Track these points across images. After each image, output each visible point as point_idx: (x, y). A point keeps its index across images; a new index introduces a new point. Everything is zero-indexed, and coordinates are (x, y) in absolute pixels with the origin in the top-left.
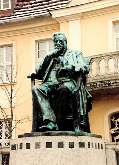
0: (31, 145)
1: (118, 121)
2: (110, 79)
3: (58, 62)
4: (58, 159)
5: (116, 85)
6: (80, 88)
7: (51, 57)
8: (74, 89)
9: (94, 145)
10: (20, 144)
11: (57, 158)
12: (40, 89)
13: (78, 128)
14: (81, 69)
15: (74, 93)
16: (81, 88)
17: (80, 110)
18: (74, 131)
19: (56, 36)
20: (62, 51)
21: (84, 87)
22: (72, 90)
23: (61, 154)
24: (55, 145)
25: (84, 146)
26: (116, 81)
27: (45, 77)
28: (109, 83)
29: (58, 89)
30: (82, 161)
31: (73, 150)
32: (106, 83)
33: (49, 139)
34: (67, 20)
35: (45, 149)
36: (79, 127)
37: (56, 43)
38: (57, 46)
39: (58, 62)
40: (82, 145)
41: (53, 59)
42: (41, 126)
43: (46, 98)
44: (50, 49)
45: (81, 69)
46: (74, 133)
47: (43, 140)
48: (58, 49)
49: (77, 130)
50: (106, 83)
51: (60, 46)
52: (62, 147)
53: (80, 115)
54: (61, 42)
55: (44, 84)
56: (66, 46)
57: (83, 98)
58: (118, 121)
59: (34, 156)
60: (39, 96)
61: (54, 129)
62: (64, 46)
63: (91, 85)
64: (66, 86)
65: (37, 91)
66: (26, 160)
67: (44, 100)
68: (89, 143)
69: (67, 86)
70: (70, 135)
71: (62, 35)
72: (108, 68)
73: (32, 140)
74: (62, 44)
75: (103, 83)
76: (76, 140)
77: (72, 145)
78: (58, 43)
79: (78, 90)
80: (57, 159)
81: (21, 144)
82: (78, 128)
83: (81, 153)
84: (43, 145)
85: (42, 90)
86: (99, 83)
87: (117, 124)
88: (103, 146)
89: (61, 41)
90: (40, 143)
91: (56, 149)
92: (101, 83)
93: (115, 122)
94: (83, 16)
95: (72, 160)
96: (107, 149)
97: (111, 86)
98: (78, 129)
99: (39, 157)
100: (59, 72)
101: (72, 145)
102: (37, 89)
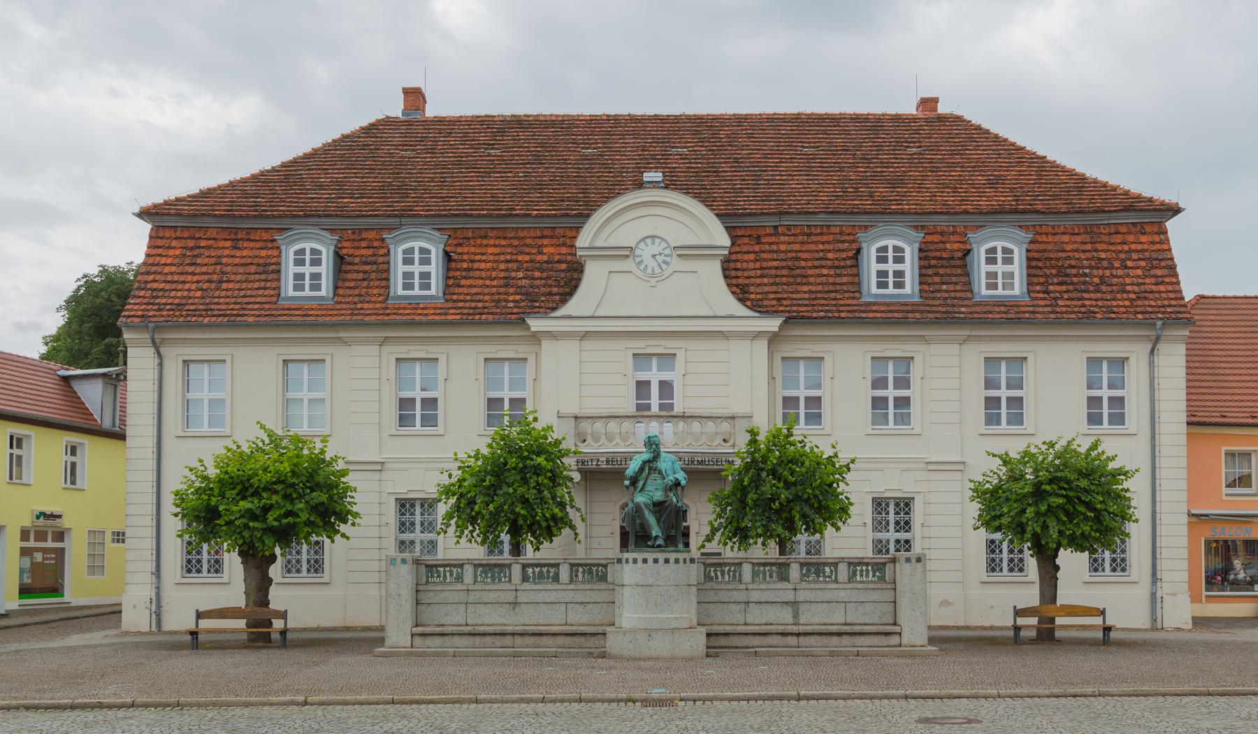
24: (672, 561)
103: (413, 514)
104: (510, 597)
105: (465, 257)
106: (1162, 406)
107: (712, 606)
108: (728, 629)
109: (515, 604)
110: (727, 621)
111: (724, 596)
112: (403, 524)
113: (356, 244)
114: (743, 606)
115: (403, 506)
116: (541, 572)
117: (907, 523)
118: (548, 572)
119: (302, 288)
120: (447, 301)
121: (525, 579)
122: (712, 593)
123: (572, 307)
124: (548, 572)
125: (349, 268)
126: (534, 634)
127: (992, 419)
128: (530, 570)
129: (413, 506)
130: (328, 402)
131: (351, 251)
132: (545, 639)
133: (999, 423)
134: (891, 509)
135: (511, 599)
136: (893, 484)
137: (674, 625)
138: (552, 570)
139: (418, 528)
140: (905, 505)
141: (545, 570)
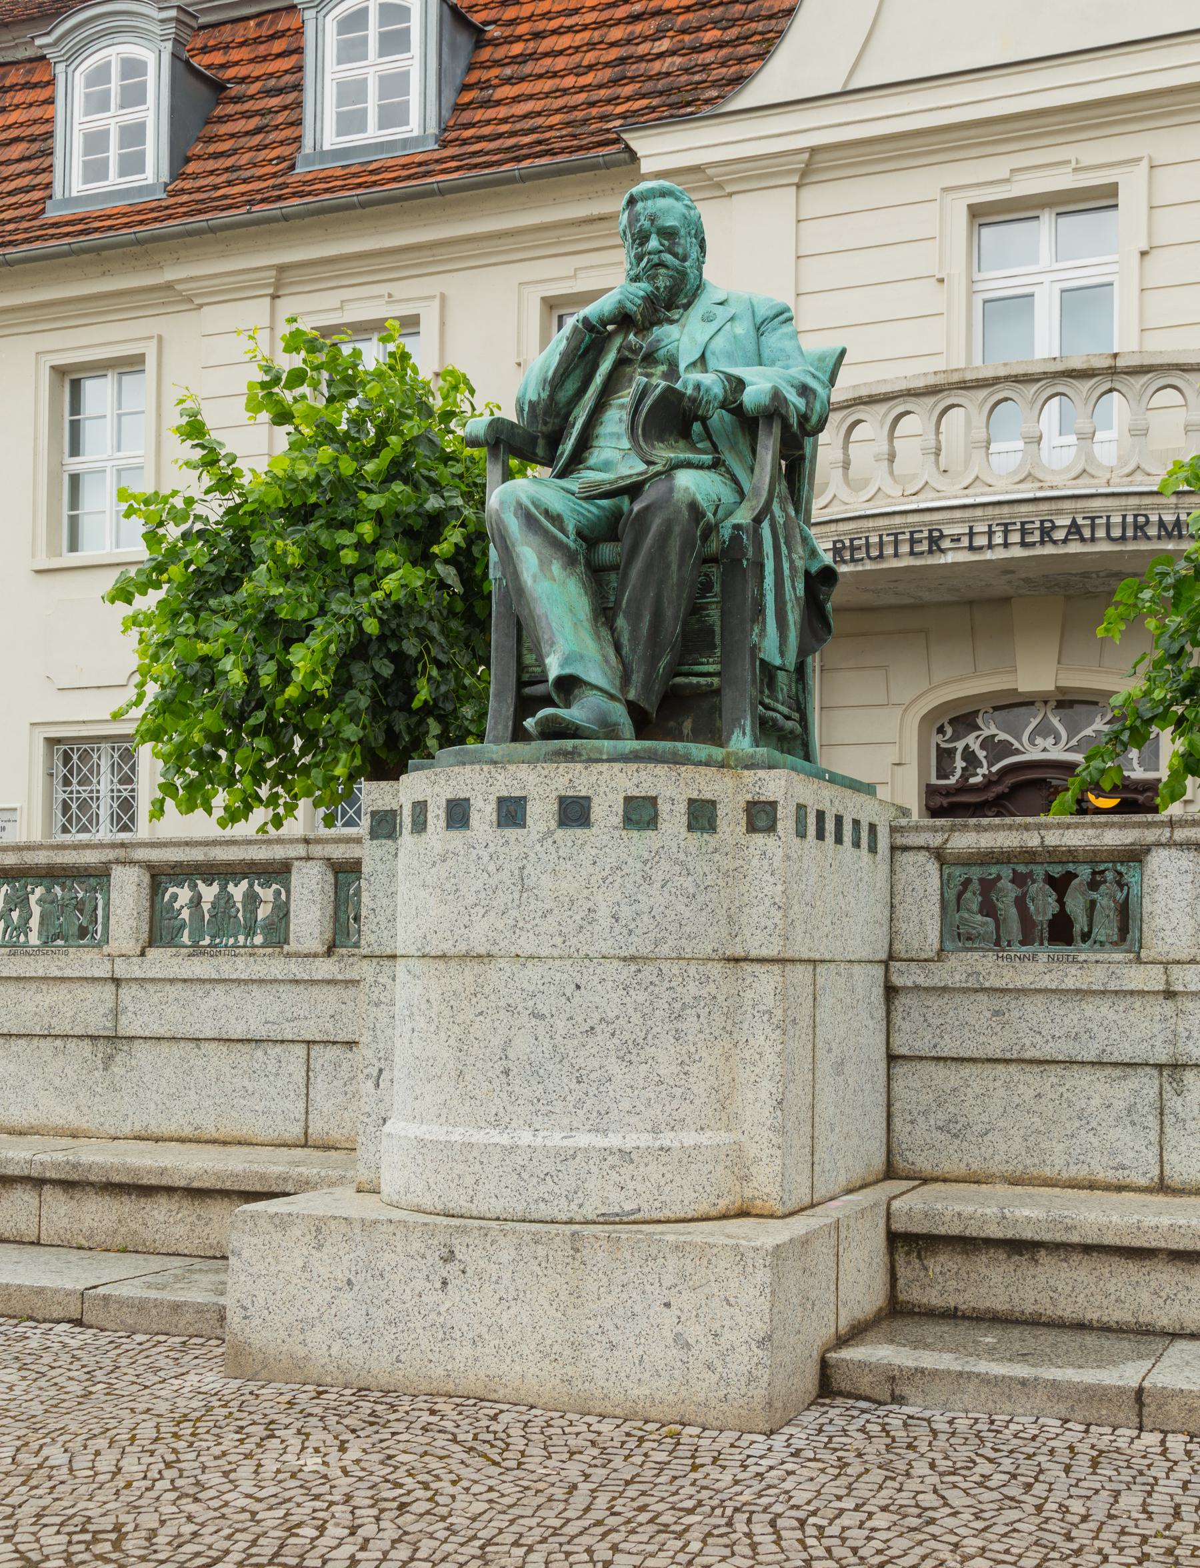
1: (967, 746)
3: (650, 359)
4: (622, 886)
5: (971, 548)
6: (767, 509)
7: (610, 328)
8: (730, 514)
9: (830, 826)
10: (416, 804)
11: (619, 880)
12: (537, 507)
13: (748, 729)
14: (777, 395)
15: (732, 538)
16: (776, 507)
18: (720, 742)
19: (639, 206)
20: (671, 288)
21: (793, 513)
22: (720, 513)
23: (639, 865)
24: (607, 810)
25: (771, 828)
26: (971, 528)
27: (568, 446)
29: (637, 507)
30: (755, 902)
31: (707, 843)
32: (916, 536)
34: (719, 186)
36: (753, 730)
37: (641, 244)
38: (643, 264)
39: (650, 359)
40: (761, 816)
41: (617, 342)
42: (533, 715)
43: (570, 559)
44: (608, 279)
45: (777, 395)
46: (718, 753)
48: (652, 279)
49: (742, 742)
50: (916, 536)
51: (661, 264)
53: (762, 661)
55: (564, 483)
56: (700, 269)
57: (787, 572)
58: (967, 746)
59: (492, 868)
60: (528, 545)
61: (610, 731)
62: (687, 264)
64: (687, 489)
66: (448, 886)
67: (556, 568)
68: (801, 807)
69: (693, 488)
70: (699, 763)
72: (937, 462)
74: (675, 255)
75: (900, 537)
76: (729, 792)
78: (654, 243)
79: (757, 520)
80: (616, 884)
81: (420, 808)
83: (755, 862)
85: (546, 513)
86: (881, 536)
87: (964, 758)
88: (880, 835)
89: (668, 234)
91: (616, 834)
92: (892, 538)
93: (956, 749)
94: (812, 166)
95: (701, 899)
96: (901, 1001)
97: (942, 551)
99: (517, 872)
100: (649, 402)
101: (702, 815)
102: (520, 505)
104: (90, 1009)
105: (522, 29)
107: (975, 1079)
108: (1029, 1213)
109: (113, 1041)
110: (1057, 1163)
111: (1041, 1028)
113: (262, 50)
114: (1147, 1085)
116: (225, 899)
118: (252, 899)
120: (444, 144)
121: (160, 931)
122: (978, 1010)
123: (773, 80)
124: (252, 899)
125: (231, 109)
126: (112, 1188)
128: (184, 895)
131: (242, 71)
132: (160, 1211)
135: (98, 1023)
137: (602, 1195)
138: (267, 894)
141: (238, 891)
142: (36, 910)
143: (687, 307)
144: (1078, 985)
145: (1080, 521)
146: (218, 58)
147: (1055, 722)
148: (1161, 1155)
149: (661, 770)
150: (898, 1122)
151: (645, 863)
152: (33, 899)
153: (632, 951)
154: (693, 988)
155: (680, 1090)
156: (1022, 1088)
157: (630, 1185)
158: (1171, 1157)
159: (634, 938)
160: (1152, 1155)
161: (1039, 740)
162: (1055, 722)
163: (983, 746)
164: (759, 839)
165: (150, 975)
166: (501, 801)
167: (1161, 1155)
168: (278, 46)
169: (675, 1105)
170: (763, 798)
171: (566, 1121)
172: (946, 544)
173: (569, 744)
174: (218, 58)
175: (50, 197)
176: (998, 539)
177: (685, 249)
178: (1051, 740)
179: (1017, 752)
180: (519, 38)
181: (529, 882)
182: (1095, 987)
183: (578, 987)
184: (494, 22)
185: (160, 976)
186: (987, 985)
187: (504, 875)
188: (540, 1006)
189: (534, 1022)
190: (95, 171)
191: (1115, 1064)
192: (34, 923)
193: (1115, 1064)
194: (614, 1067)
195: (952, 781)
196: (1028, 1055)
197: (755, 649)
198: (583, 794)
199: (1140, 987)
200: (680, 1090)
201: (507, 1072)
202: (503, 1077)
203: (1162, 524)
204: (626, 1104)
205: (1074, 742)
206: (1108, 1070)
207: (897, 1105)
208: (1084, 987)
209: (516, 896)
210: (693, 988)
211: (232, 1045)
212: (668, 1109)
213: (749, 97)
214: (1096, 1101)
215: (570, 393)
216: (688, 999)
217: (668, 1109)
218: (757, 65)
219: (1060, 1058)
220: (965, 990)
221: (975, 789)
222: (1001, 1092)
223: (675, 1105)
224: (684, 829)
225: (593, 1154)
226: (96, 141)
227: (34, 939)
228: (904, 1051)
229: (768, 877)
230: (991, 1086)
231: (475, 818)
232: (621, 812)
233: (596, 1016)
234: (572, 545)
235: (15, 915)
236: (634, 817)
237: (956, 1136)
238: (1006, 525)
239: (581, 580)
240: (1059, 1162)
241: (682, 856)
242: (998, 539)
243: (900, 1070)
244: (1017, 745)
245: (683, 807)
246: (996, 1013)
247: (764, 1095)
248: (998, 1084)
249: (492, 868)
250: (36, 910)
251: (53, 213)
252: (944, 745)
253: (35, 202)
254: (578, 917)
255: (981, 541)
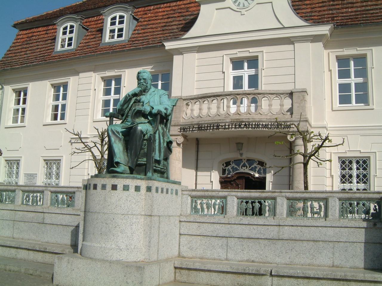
0: (97, 186)
2: (220, 121)
10: (168, 193)
12: (114, 130)
13: (151, 172)
17: (155, 154)
23: (125, 197)
24: (120, 187)
25: (150, 191)
26: (225, 124)
28: (259, 124)
33: (115, 181)
35: (110, 191)
47: (109, 181)
52: (128, 190)
53: (155, 159)
54: (144, 81)
59: (100, 197)
63: (199, 126)
65: (111, 131)
67: (117, 142)
71: (147, 73)
73: (100, 182)
76: (143, 184)
77: (137, 189)
78: (142, 81)
82: (151, 172)
84: (109, 187)
87: (236, 168)
90: (106, 185)
91: (122, 192)
93: (226, 169)
98: (151, 173)
101: (137, 189)
103: (351, 169)
106: (371, 89)
112: (343, 176)
113: (96, 22)
115: (343, 162)
117: (365, 176)
119: (113, 37)
121: (292, 211)
123: (193, 31)
127: (344, 99)
129: (351, 162)
130: (15, 125)
133: (350, 102)
134: (355, 166)
136: (356, 147)
139: (355, 180)
140: (364, 163)
142: (31, 198)
143: (147, 92)
144: (213, 222)
145: (247, 124)
146: (88, 24)
147: (246, 164)
148: (227, 254)
149: (130, 180)
150: (181, 247)
151: (126, 197)
152: (31, 196)
153: (123, 213)
154: (134, 220)
155: (131, 239)
156: (203, 241)
157: (121, 255)
158: (229, 255)
159: (124, 211)
160: (225, 254)
161: (243, 167)
162: (246, 164)
163: (232, 169)
164: (148, 193)
165: (50, 212)
166: (102, 184)
167: (227, 254)
168: (99, 22)
169: (130, 241)
170: (149, 186)
171: (111, 243)
172: (220, 127)
173: (115, 174)
174: (88, 24)
175: (54, 51)
176: (231, 127)
177: (147, 82)
178: (245, 168)
179: (239, 170)
180: (146, 21)
181: (106, 200)
182: (216, 222)
183: (114, 219)
184: (141, 18)
185: (51, 212)
186: (197, 221)
187: (102, 198)
188: (107, 222)
189: (106, 225)
190: (63, 46)
191: (220, 237)
192: (31, 200)
193: (220, 237)
194: (120, 234)
195: (225, 176)
196: (204, 235)
197: (153, 157)
198: (116, 184)
199: (224, 222)
200: (131, 239)
201: (101, 234)
202: (100, 234)
203: (263, 125)
204: (121, 241)
205: (250, 168)
206: (218, 238)
207: (181, 243)
208: (214, 222)
209: (104, 202)
210: (134, 220)
211: (63, 226)
212: (129, 242)
213: (187, 35)
214: (216, 244)
215: (126, 107)
216: (133, 222)
217: (129, 242)
218: (180, 36)
219: (210, 235)
220: (193, 222)
221: (229, 178)
222: (199, 242)
223: (130, 241)
224: (134, 191)
225: (115, 249)
226: (63, 40)
227: (30, 204)
228: (182, 233)
229: (149, 200)
230: (198, 240)
231: (98, 188)
232: (122, 187)
233: (117, 224)
234: (120, 137)
235: (27, 199)
236: (125, 189)
237: (191, 250)
238: (232, 124)
239: (122, 144)
240: (209, 255)
241: (133, 196)
242: (231, 127)
243: (182, 237)
244: (238, 168)
245: (134, 187)
246: (199, 227)
247: (147, 240)
248: (199, 240)
249: (100, 197)
250: (31, 198)
251: (53, 54)
252: (224, 168)
253: (51, 52)
254: (114, 206)
255: (227, 127)
